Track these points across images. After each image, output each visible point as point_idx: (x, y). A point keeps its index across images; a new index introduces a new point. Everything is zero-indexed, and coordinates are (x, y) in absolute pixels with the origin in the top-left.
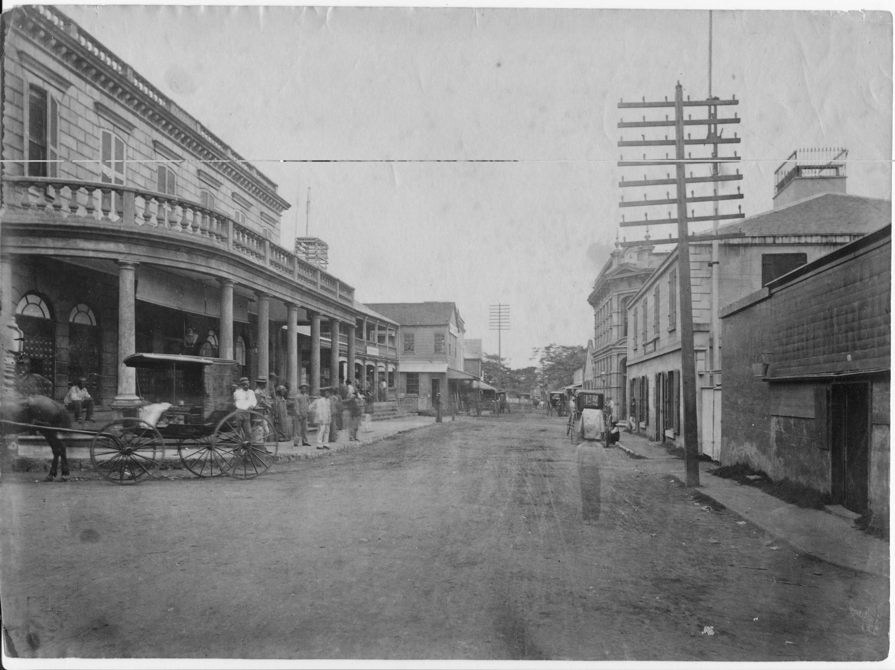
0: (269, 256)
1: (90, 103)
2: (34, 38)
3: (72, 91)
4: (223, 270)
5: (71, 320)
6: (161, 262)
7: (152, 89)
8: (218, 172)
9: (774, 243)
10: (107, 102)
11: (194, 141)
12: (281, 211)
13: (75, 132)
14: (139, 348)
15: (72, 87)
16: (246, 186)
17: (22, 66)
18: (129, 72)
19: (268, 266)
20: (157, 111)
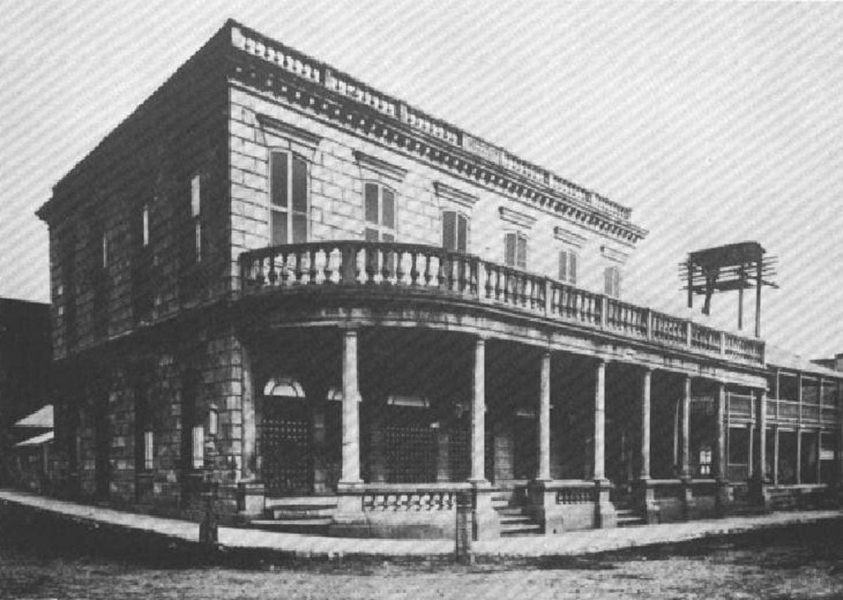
0: (724, 348)
1: (347, 153)
2: (460, 172)
3: (324, 146)
4: (470, 325)
5: (60, 355)
6: (570, 349)
7: (268, 43)
8: (455, 176)
9: (241, 426)
10: (369, 149)
11: (456, 158)
12: (635, 241)
13: (330, 191)
14: (781, 433)
15: (322, 142)
16: (512, 190)
17: (263, 131)
18: (403, 110)
19: (725, 357)
20: (483, 167)
